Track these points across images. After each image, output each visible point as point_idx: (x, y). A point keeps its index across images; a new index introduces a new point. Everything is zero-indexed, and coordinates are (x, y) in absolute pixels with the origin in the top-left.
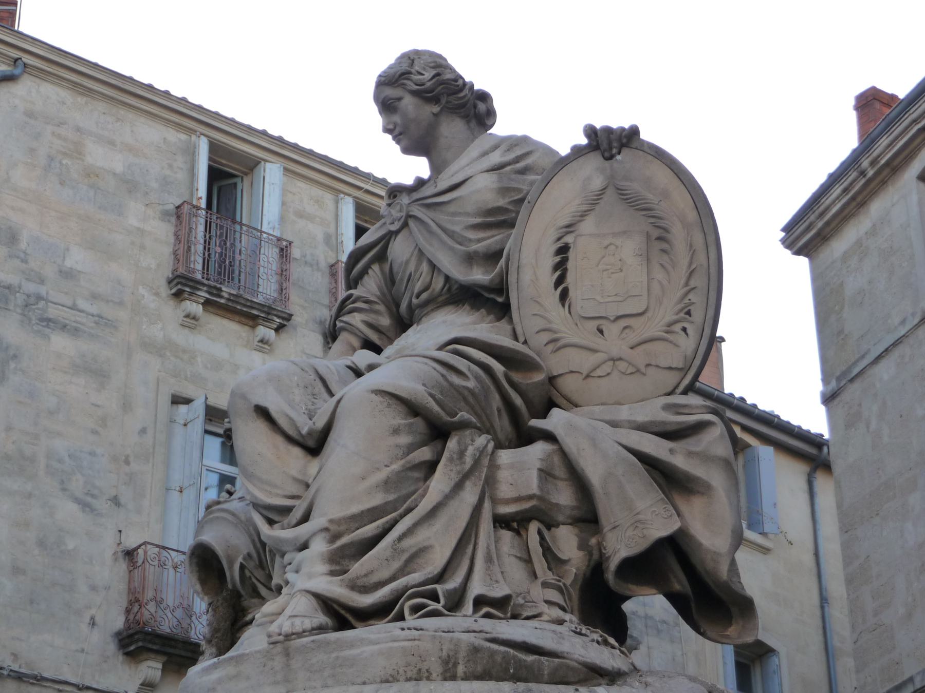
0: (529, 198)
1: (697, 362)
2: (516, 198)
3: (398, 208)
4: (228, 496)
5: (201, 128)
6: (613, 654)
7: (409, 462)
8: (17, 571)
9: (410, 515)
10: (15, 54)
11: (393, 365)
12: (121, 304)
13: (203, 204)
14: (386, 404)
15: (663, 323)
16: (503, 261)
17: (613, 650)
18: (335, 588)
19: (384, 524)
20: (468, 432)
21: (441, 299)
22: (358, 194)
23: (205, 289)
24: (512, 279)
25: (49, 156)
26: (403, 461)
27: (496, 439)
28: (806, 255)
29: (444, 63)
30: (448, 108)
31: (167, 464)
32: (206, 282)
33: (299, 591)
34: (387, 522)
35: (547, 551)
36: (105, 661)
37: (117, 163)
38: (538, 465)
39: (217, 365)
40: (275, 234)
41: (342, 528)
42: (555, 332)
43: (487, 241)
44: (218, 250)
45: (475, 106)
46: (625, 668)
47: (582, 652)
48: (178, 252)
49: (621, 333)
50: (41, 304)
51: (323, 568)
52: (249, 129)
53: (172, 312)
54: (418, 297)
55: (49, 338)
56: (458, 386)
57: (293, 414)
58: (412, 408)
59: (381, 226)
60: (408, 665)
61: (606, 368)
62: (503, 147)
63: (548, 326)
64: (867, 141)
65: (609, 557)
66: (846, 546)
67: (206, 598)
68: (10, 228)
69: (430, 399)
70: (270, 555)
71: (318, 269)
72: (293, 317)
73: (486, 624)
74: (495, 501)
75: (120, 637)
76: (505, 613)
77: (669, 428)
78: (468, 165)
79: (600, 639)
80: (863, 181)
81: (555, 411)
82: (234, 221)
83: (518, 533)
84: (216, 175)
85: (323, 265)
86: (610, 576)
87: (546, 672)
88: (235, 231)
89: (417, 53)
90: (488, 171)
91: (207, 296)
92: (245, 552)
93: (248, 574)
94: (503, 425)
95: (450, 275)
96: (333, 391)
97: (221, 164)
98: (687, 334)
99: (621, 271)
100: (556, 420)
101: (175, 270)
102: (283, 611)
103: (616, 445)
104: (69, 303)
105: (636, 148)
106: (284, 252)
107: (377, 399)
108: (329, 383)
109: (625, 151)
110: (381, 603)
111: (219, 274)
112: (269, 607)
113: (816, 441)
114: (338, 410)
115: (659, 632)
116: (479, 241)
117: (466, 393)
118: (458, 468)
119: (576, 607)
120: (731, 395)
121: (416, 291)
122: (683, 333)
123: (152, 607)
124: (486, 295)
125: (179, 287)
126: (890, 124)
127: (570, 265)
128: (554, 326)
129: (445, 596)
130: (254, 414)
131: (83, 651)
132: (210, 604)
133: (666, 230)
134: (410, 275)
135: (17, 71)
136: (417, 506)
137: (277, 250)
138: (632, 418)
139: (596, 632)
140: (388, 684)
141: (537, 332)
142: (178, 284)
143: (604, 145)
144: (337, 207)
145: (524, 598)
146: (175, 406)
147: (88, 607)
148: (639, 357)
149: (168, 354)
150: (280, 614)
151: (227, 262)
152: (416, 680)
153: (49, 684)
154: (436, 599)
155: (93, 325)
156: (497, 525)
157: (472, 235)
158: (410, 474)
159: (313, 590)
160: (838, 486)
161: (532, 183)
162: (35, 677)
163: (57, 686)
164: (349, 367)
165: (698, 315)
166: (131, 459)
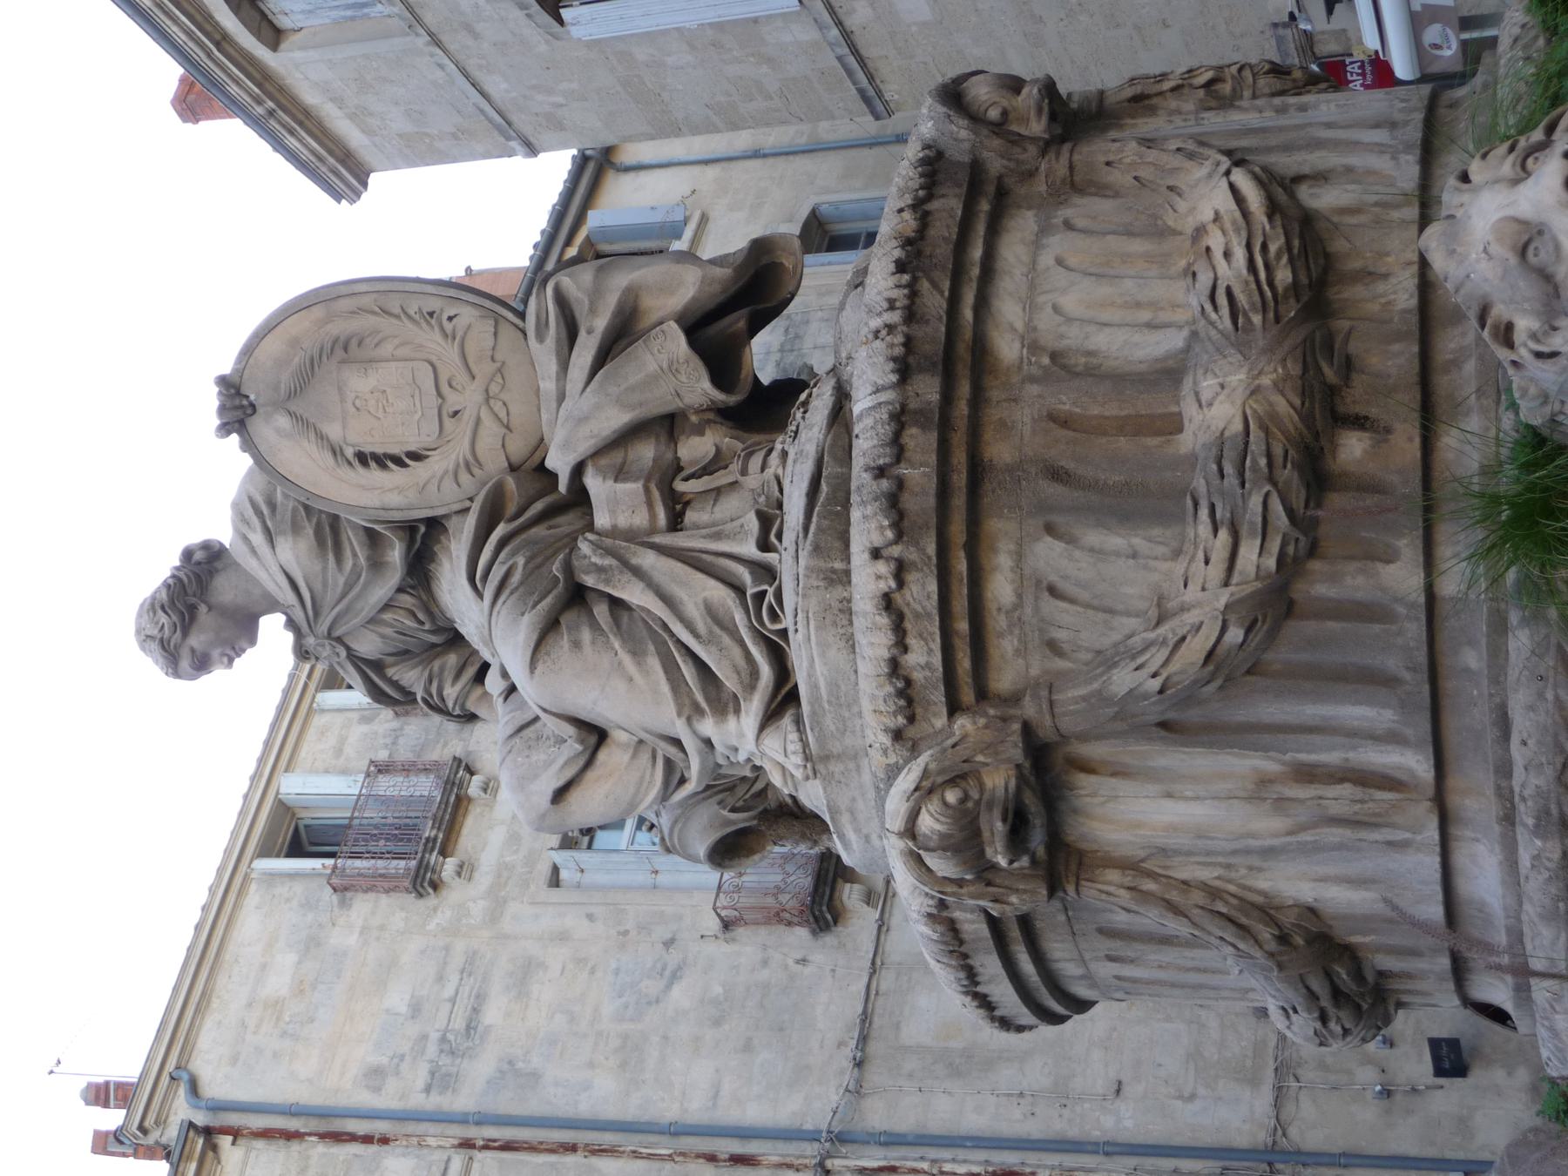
0: (303, 499)
1: (488, 303)
2: (303, 513)
3: (320, 649)
4: (655, 829)
5: (243, 868)
6: (818, 395)
7: (611, 631)
8: (748, 1047)
9: (671, 626)
10: (165, 1079)
11: (501, 649)
12: (447, 949)
13: (330, 862)
14: (546, 657)
15: (443, 343)
16: (376, 527)
17: (814, 395)
18: (753, 709)
19: (681, 655)
20: (576, 563)
21: (424, 597)
23: (427, 856)
24: (398, 516)
25: (282, 1036)
26: (611, 636)
27: (583, 531)
28: (368, 176)
29: (148, 601)
30: (202, 594)
31: (627, 888)
32: (419, 855)
33: (757, 745)
34: (679, 652)
35: (707, 470)
36: (844, 945)
37: (286, 960)
38: (610, 482)
39: (514, 839)
40: (362, 780)
41: (687, 701)
42: (458, 465)
43: (354, 544)
44: (382, 843)
45: (199, 563)
46: (832, 382)
47: (816, 430)
48: (386, 887)
49: (457, 390)
50: (451, 1037)
51: (732, 722)
52: (242, 813)
53: (457, 893)
54: (422, 623)
55: (490, 1026)
56: (523, 575)
57: (561, 761)
58: (550, 627)
59: (342, 667)
60: (835, 624)
61: (498, 407)
63: (451, 473)
64: (236, 108)
65: (711, 400)
66: (696, 130)
67: (769, 848)
68: (365, 1075)
69: (539, 607)
70: (719, 779)
71: (401, 729)
72: (457, 755)
73: (789, 537)
74: (653, 530)
75: (818, 930)
76: (776, 516)
77: (564, 335)
78: (267, 570)
79: (802, 410)
80: (280, 112)
81: (549, 464)
82: (349, 827)
83: (687, 503)
84: (296, 849)
86: (732, 400)
87: (839, 470)
88: (360, 825)
89: (138, 632)
90: (273, 547)
91: (435, 853)
92: (717, 807)
93: (741, 803)
94: (567, 522)
95: (396, 587)
96: (533, 716)
97: (283, 843)
98: (456, 316)
99: (385, 391)
100: (559, 462)
101: (407, 891)
102: (779, 763)
103: (585, 394)
105: (241, 377)
106: (382, 769)
108: (524, 722)
109: (244, 391)
110: (768, 655)
111: (409, 840)
112: (776, 779)
113: (581, 162)
114: (554, 710)
115: (797, 336)
116: (355, 555)
117: (531, 566)
118: (616, 573)
119: (768, 437)
120: (531, 258)
121: (416, 625)
122: (455, 320)
123: (784, 898)
125: (426, 884)
127: (379, 450)
128: (451, 467)
129: (760, 584)
130: (562, 804)
131: (833, 971)
132: (775, 844)
133: (335, 342)
134: (397, 632)
135: (185, 1076)
136: (660, 619)
137: (381, 776)
138: (554, 375)
139: (794, 414)
140: (857, 645)
141: (459, 486)
142: (422, 886)
143: (239, 414)
144: (329, 710)
145: (759, 495)
146: (561, 883)
147: (786, 967)
148: (483, 369)
149: (503, 893)
150: (783, 767)
151: (397, 832)
152: (851, 614)
153: (870, 1006)
154: (761, 595)
155: (472, 979)
156: (679, 527)
157: (349, 564)
158: (624, 627)
159: (756, 731)
160: (630, 139)
161: (286, 496)
162: (863, 1021)
163: (872, 997)
166: (622, 929)
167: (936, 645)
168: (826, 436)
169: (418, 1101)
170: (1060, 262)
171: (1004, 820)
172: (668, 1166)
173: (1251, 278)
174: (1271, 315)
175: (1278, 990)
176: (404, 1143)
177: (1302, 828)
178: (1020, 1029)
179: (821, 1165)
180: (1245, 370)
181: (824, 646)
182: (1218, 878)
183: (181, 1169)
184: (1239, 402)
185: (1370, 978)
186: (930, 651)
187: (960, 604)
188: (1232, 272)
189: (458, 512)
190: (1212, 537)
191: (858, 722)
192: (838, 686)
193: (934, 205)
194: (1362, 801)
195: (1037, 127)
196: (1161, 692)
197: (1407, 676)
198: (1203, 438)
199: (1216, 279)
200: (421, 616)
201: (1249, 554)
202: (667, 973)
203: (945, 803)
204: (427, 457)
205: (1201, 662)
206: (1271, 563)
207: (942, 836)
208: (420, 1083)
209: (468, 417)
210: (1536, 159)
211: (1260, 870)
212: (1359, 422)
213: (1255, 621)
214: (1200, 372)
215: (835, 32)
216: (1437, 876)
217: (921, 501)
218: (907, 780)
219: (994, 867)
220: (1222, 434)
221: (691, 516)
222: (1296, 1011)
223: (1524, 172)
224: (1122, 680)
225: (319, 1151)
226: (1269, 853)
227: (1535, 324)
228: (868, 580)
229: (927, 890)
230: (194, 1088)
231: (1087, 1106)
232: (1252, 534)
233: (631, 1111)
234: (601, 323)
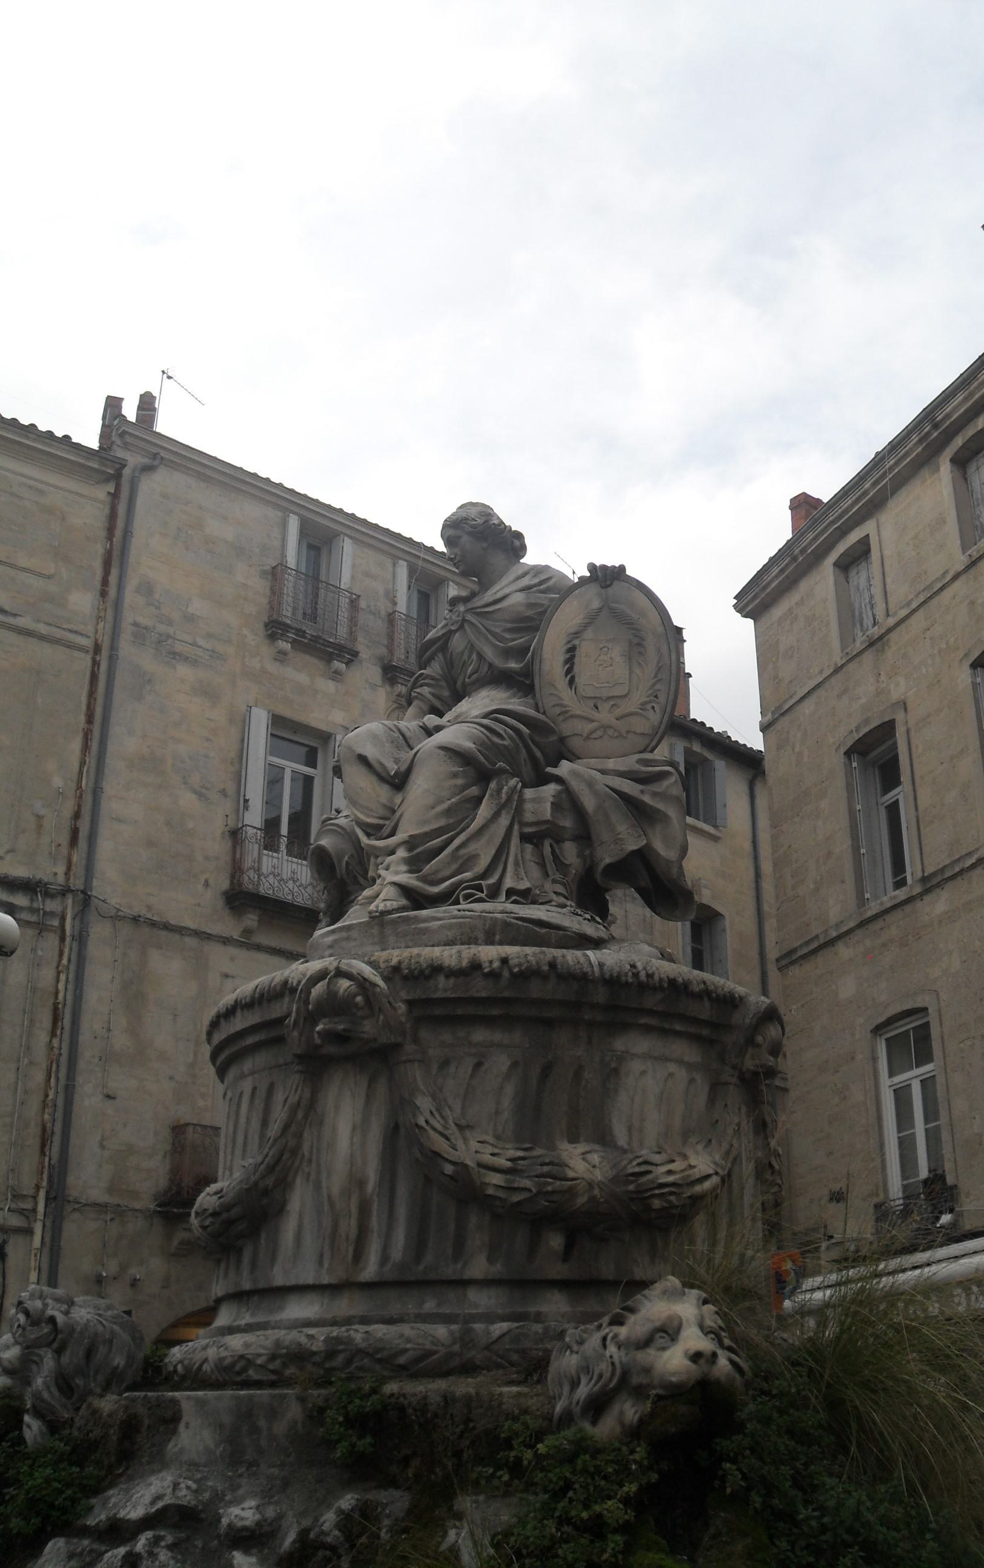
3: (457, 614)
5: (293, 508)
10: (155, 450)
15: (639, 702)
16: (530, 654)
19: (446, 839)
24: (536, 668)
38: (551, 799)
42: (565, 706)
45: (512, 542)
50: (170, 641)
53: (267, 650)
54: (469, 678)
60: (462, 934)
61: (599, 733)
62: (532, 574)
63: (560, 702)
64: (799, 533)
67: (322, 884)
72: (360, 654)
76: (527, 900)
83: (536, 845)
85: (383, 613)
86: (598, 876)
90: (520, 591)
93: (351, 868)
94: (527, 770)
100: (564, 768)
104: (190, 641)
105: (624, 581)
106: (354, 603)
109: (616, 583)
124: (518, 678)
126: (815, 522)
127: (576, 660)
135: (156, 463)
142: (272, 627)
154: (479, 888)
157: (507, 636)
161: (551, 599)
164: (421, 727)
165: (662, 698)
167: (449, 994)
168: (575, 933)
169: (128, 617)
170: (671, 1075)
171: (344, 1030)
172: (74, 786)
173: (655, 1185)
174: (635, 1196)
175: (234, 1187)
176: (101, 607)
177: (332, 1204)
178: (210, 1034)
179: (69, 890)
180: (603, 1180)
181: (450, 927)
182: (303, 1155)
183: (96, 458)
184: (585, 1176)
186: (445, 990)
189: (537, 704)
190: (507, 1158)
191: (403, 945)
192: (424, 934)
193: (707, 1004)
194: (347, 1239)
195: (749, 1064)
196: (417, 1125)
197: (421, 1267)
198: (565, 1156)
199: (657, 1165)
201: (496, 1179)
202: (204, 791)
204: (571, 688)
205: (434, 1149)
206: (490, 1191)
207: (336, 993)
208: (140, 620)
209: (596, 715)
210: (714, 1339)
211: (308, 1179)
212: (569, 1248)
213: (456, 1181)
214: (603, 1154)
215: (834, 934)
216: (301, 1282)
217: (535, 990)
218: (367, 971)
219: (316, 1024)
220: (567, 1166)
221: (529, 847)
222: (220, 1198)
223: (706, 1331)
224: (424, 1103)
225: (100, 549)
226: (318, 1186)
227: (622, 1337)
229: (303, 982)
230: (148, 469)
231: (99, 1075)
232: (507, 1181)
233: (114, 763)
234: (647, 799)
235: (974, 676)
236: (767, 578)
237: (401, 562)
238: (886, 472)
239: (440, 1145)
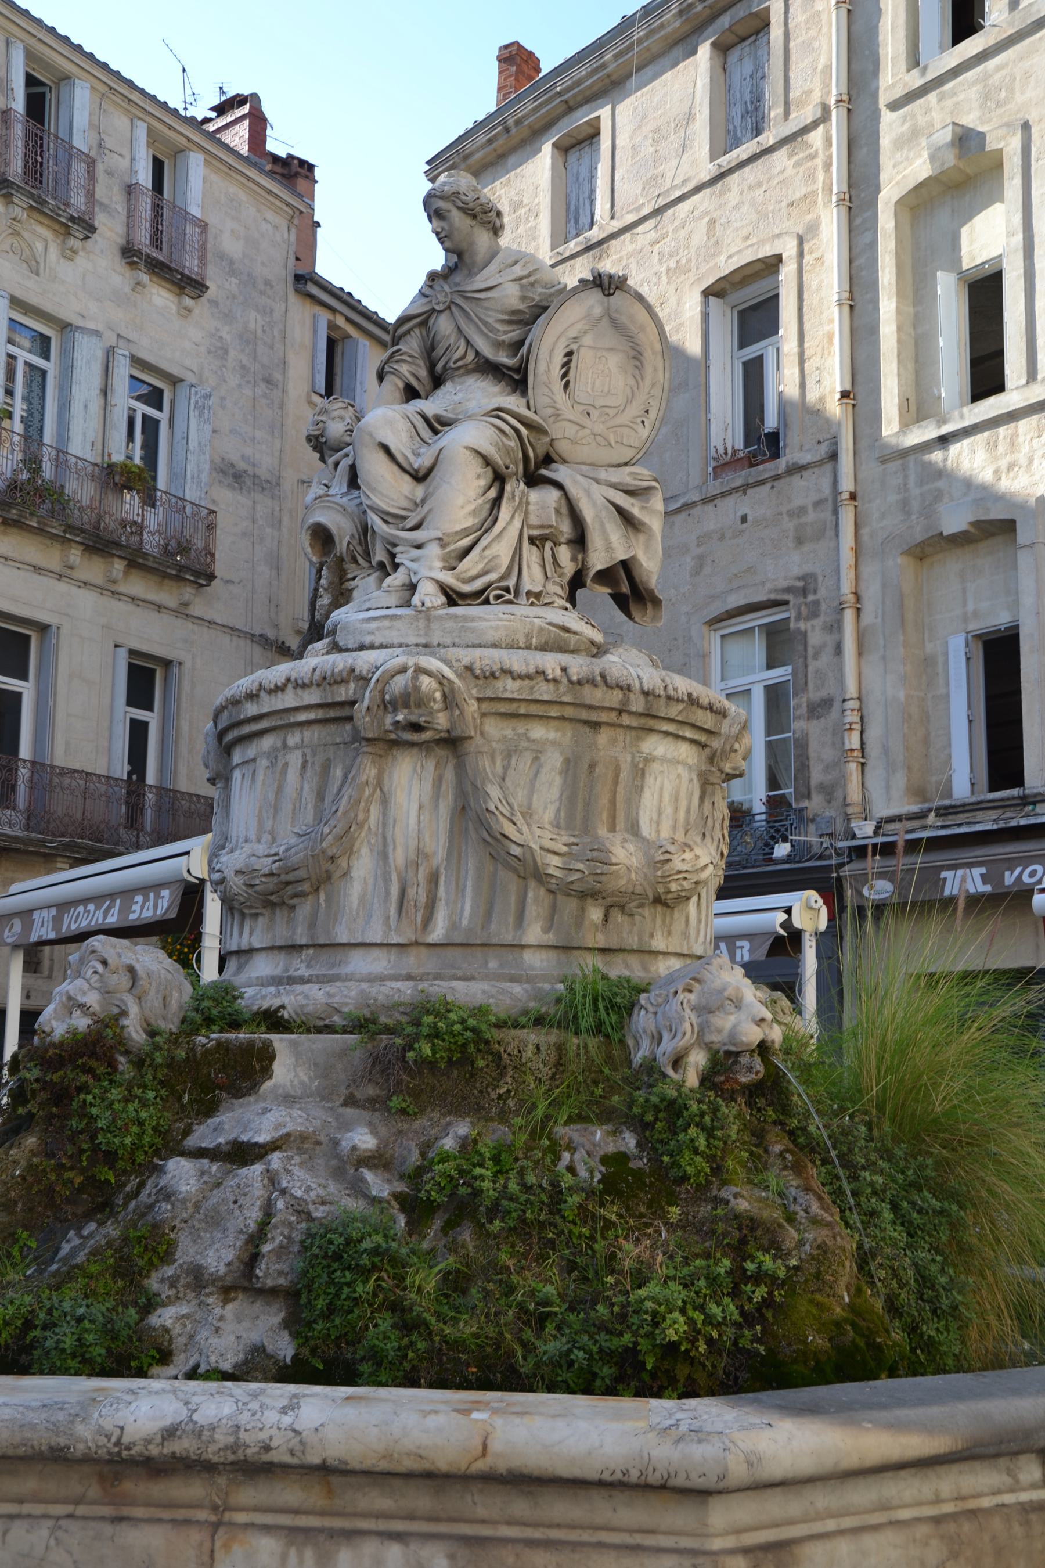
18: (448, 578)
22: (32, 41)
24: (531, 367)
62: (521, 263)
107: (468, 453)
115: (263, 489)
127: (573, 365)
157: (501, 327)
167: (515, 696)
185: (295, 901)
187: (534, 709)
188: (677, 864)
200: (460, 363)
201: (556, 861)
203: (434, 691)
206: (551, 871)
209: (585, 421)
228: (551, 662)
232: (564, 863)
234: (636, 511)
235: (706, 304)
236: (469, 146)
237: (140, 123)
238: (633, 43)
239: (509, 830)
